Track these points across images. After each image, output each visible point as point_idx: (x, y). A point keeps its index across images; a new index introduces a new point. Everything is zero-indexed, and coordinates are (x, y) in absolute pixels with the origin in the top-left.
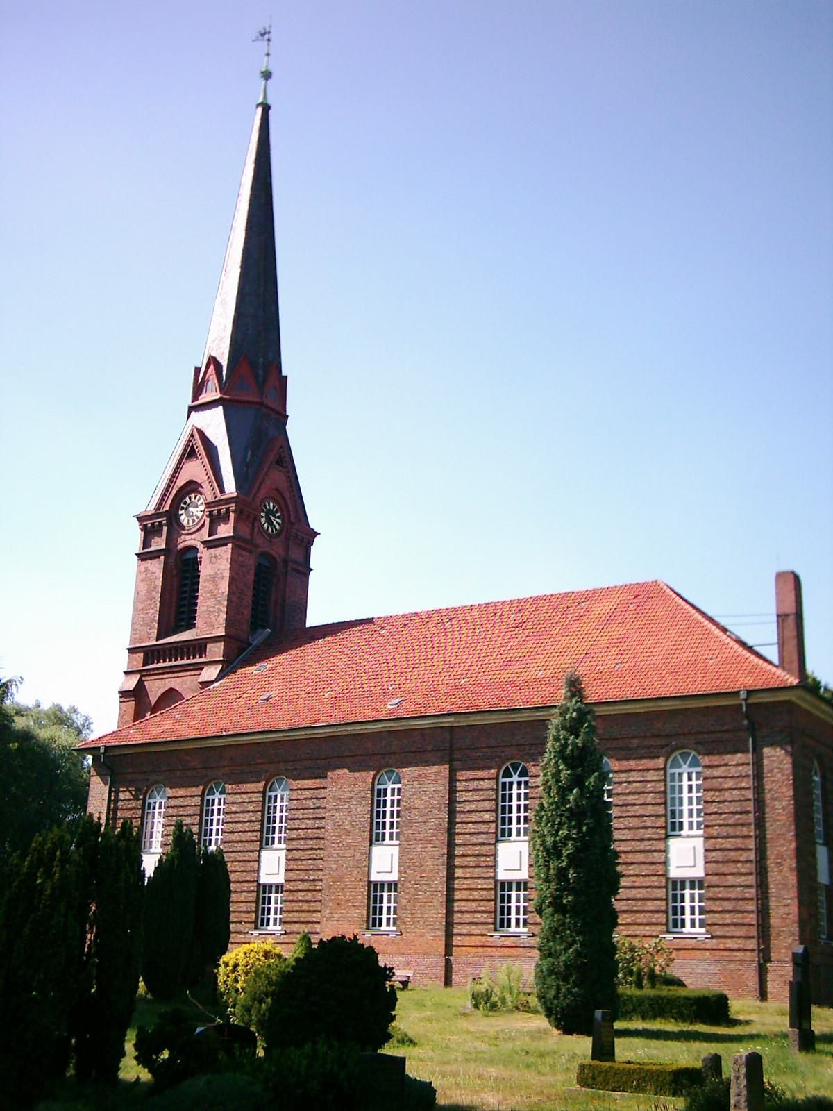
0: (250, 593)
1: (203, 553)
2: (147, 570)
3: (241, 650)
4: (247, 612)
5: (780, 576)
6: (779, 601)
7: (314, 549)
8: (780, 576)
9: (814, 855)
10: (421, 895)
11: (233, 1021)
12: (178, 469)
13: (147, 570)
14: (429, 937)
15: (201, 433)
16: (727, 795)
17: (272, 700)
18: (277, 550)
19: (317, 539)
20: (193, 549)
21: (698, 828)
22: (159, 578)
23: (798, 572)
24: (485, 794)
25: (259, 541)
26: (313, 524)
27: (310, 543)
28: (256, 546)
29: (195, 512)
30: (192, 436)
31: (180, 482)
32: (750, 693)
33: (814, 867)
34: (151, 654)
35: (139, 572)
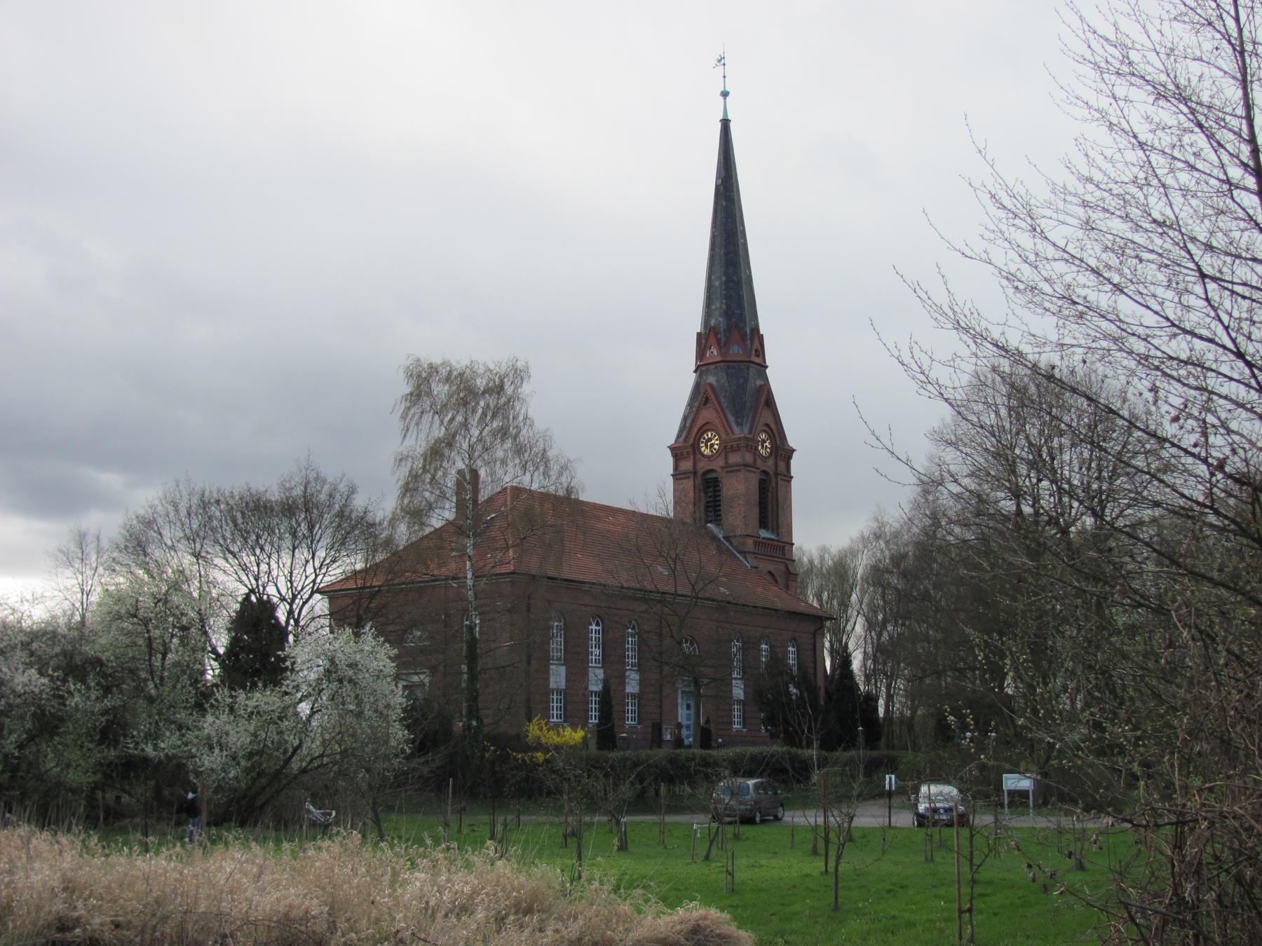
7: (792, 462)
20: (712, 471)
27: (790, 458)
31: (699, 423)
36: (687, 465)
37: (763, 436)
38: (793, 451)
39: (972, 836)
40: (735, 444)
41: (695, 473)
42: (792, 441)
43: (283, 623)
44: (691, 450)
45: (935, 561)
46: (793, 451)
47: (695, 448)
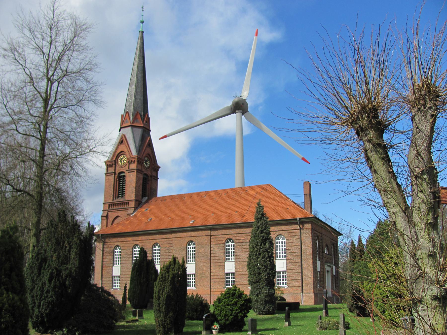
0: (141, 186)
1: (126, 174)
2: (108, 179)
3: (139, 204)
4: (141, 192)
5: (305, 183)
6: (304, 191)
7: (159, 172)
8: (305, 183)
9: (316, 263)
10: (202, 278)
11: (8, 195)
12: (117, 148)
13: (108, 179)
14: (205, 289)
15: (124, 135)
16: (293, 248)
17: (152, 220)
18: (149, 173)
19: (160, 169)
20: (123, 172)
21: (285, 257)
22: (133, 192)
23: (310, 182)
24: (221, 248)
25: (144, 170)
26: (159, 164)
27: (158, 170)
28: (143, 172)
29: (123, 160)
30: (122, 137)
31: (118, 152)
32: (300, 219)
33: (316, 267)
34: (110, 205)
35: (106, 180)
36: (111, 170)
37: (147, 159)
38: (159, 167)
39: (14, 188)
40: (133, 160)
41: (115, 173)
42: (159, 163)
43: (121, 302)
44: (114, 163)
45: (168, 327)
46: (159, 167)
47: (116, 162)
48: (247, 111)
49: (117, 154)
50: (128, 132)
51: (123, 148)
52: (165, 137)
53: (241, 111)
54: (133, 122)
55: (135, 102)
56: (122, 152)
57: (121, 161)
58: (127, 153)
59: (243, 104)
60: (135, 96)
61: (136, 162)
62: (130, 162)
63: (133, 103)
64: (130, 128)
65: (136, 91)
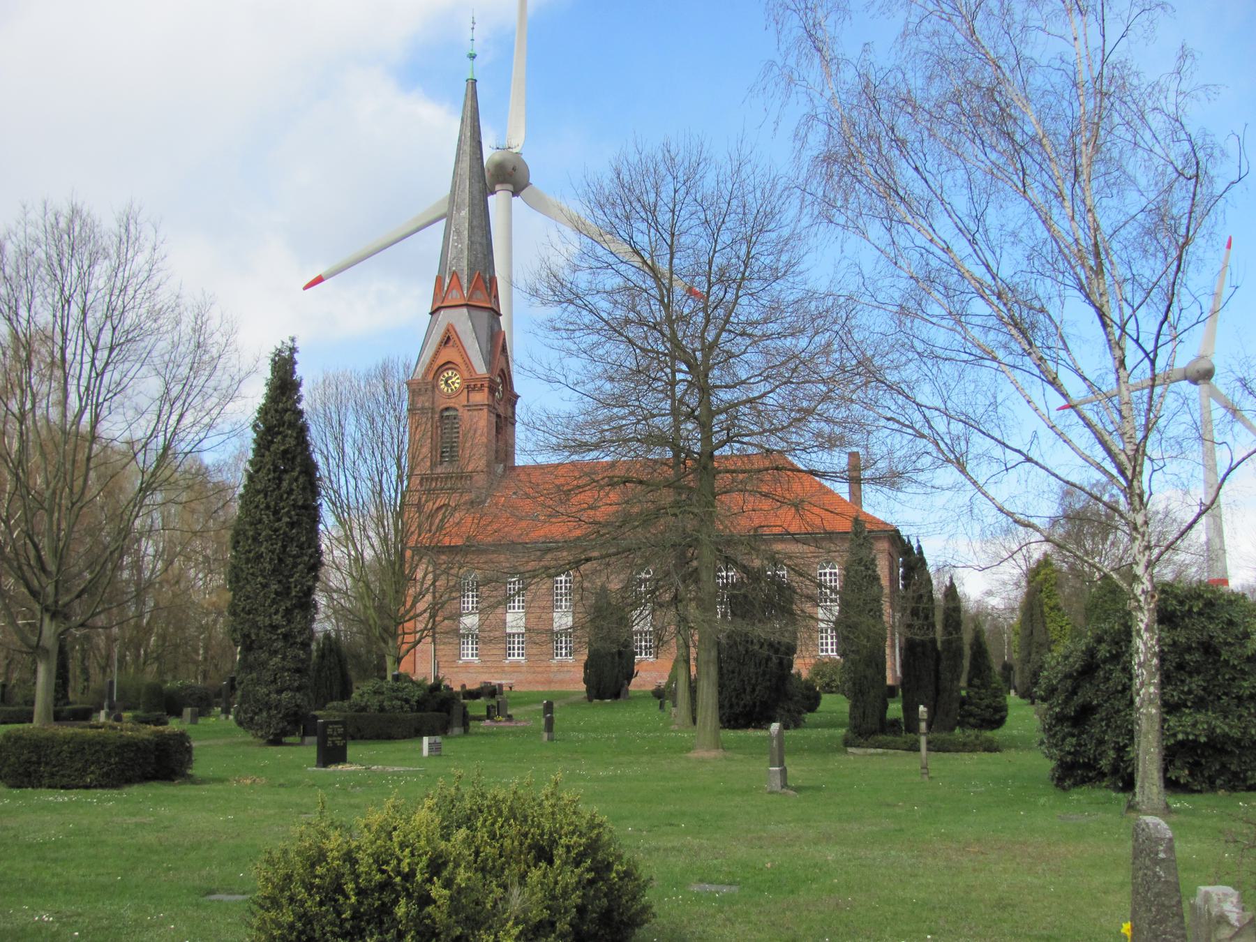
31: (440, 361)
48: (527, 184)
49: (435, 367)
50: (461, 320)
51: (449, 354)
52: (319, 280)
53: (510, 187)
54: (470, 298)
55: (470, 249)
56: (449, 362)
57: (446, 382)
58: (463, 367)
59: (514, 169)
60: (470, 237)
61: (486, 390)
62: (470, 388)
63: (466, 253)
64: (465, 310)
65: (471, 227)
